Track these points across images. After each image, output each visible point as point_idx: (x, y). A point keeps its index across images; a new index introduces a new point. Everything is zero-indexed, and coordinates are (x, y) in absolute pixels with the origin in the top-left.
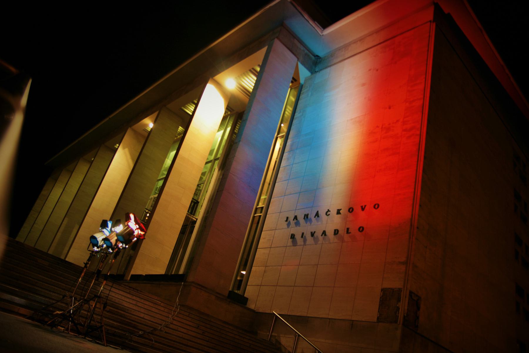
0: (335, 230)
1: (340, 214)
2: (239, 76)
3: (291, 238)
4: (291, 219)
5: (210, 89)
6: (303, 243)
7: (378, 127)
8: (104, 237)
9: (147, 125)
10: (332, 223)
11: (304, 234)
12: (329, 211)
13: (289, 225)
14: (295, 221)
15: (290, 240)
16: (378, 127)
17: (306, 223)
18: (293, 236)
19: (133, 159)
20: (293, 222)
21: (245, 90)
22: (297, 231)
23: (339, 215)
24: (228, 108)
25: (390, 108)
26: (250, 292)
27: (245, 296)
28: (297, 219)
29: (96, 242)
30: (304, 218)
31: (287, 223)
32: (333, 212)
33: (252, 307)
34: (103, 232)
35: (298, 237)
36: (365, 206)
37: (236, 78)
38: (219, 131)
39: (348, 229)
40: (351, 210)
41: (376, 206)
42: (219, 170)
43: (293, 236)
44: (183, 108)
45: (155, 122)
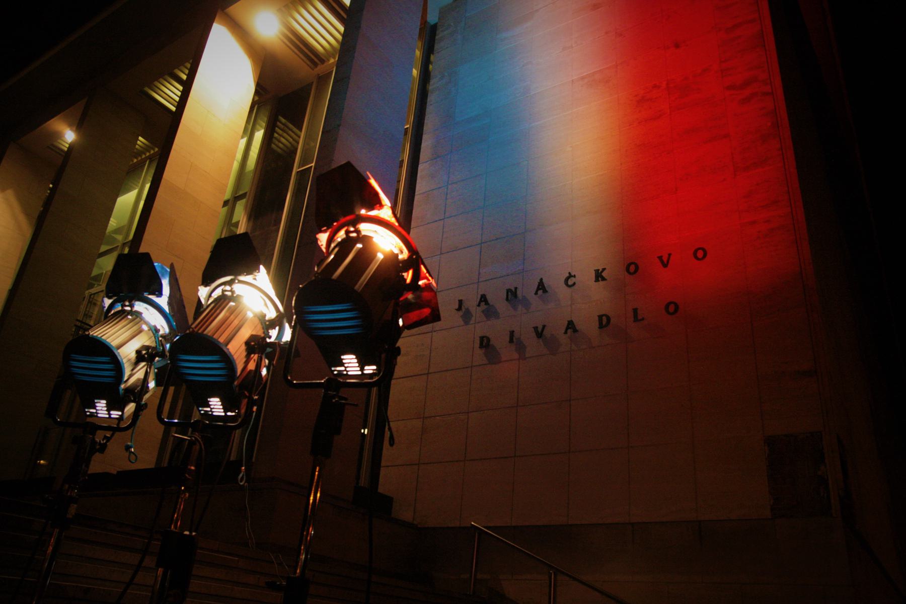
0: (600, 317)
1: (604, 279)
2: (286, 6)
3: (481, 346)
4: (472, 303)
5: (219, 38)
6: (516, 356)
7: (655, 86)
8: (143, 340)
9: (59, 135)
10: (590, 301)
11: (516, 335)
12: (570, 276)
13: (467, 316)
14: (483, 306)
15: (479, 352)
16: (655, 86)
17: (515, 308)
18: (485, 343)
19: (27, 214)
20: (477, 312)
21: (300, 45)
22: (497, 330)
23: (601, 283)
24: (260, 90)
25: (677, 46)
26: (388, 482)
27: (381, 490)
28: (486, 302)
29: (105, 373)
30: (507, 299)
31: (461, 313)
32: (585, 277)
33: (406, 515)
34: (138, 315)
35: (500, 343)
36: (516, 288)
37: (280, 10)
38: (242, 137)
39: (635, 311)
40: (632, 268)
41: (700, 254)
42: (249, 219)
43: (485, 343)
44: (146, 89)
45: (79, 127)
